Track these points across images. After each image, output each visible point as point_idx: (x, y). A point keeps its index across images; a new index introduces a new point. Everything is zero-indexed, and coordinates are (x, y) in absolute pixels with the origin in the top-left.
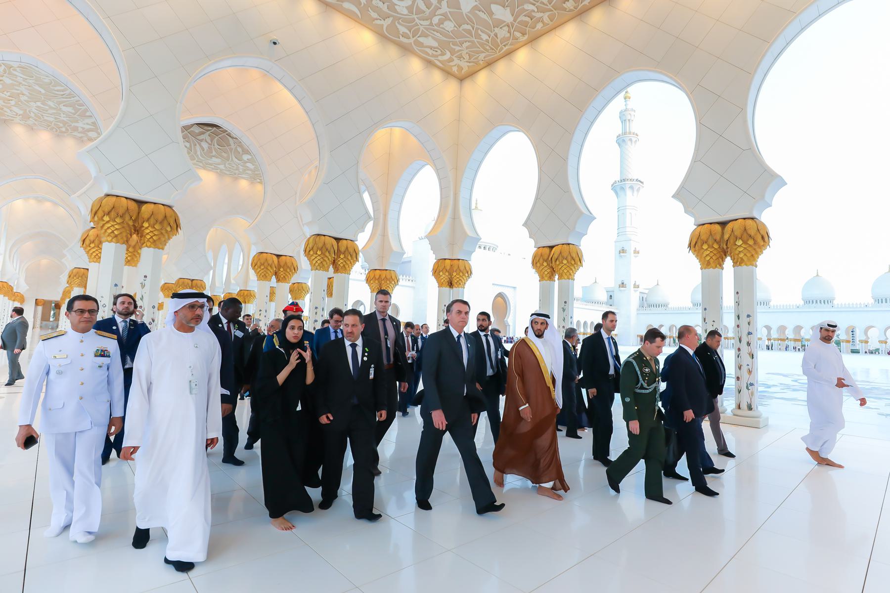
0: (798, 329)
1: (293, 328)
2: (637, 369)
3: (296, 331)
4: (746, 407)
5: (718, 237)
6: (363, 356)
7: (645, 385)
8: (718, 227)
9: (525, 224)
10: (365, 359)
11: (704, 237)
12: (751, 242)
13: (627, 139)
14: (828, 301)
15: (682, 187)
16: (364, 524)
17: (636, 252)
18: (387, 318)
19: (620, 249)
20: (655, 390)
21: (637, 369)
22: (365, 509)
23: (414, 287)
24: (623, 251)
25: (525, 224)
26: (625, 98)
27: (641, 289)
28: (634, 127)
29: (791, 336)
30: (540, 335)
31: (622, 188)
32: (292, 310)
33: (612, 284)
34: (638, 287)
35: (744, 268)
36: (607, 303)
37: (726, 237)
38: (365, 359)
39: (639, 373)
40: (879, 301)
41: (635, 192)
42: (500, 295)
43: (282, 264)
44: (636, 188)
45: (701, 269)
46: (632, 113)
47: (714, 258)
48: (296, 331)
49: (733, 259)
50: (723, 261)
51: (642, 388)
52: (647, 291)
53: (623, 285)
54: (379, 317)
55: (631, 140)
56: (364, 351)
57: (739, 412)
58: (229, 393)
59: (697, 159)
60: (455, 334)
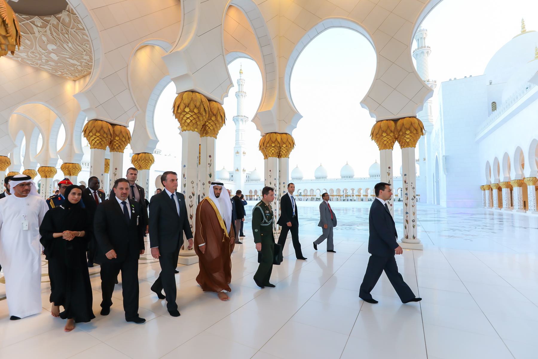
0: (359, 190)
1: (74, 194)
2: (262, 212)
3: (76, 196)
4: (412, 238)
5: (393, 129)
6: (132, 210)
7: (267, 221)
8: (392, 123)
10: (133, 212)
11: (384, 128)
12: (415, 132)
13: (240, 95)
14: (351, 177)
15: (368, 96)
16: (133, 326)
17: (244, 153)
18: (135, 185)
21: (262, 212)
22: (133, 315)
24: (238, 153)
27: (247, 172)
28: (245, 89)
29: (309, 194)
30: (217, 196)
31: (237, 120)
32: (65, 183)
33: (232, 169)
35: (410, 149)
37: (399, 128)
38: (133, 212)
39: (263, 214)
40: (317, 178)
41: (244, 123)
43: (117, 133)
45: (380, 150)
46: (243, 81)
47: (389, 142)
48: (76, 196)
49: (399, 142)
50: (394, 143)
51: (265, 223)
53: (237, 170)
56: (131, 207)
57: (406, 240)
59: (377, 79)
60: (170, 194)
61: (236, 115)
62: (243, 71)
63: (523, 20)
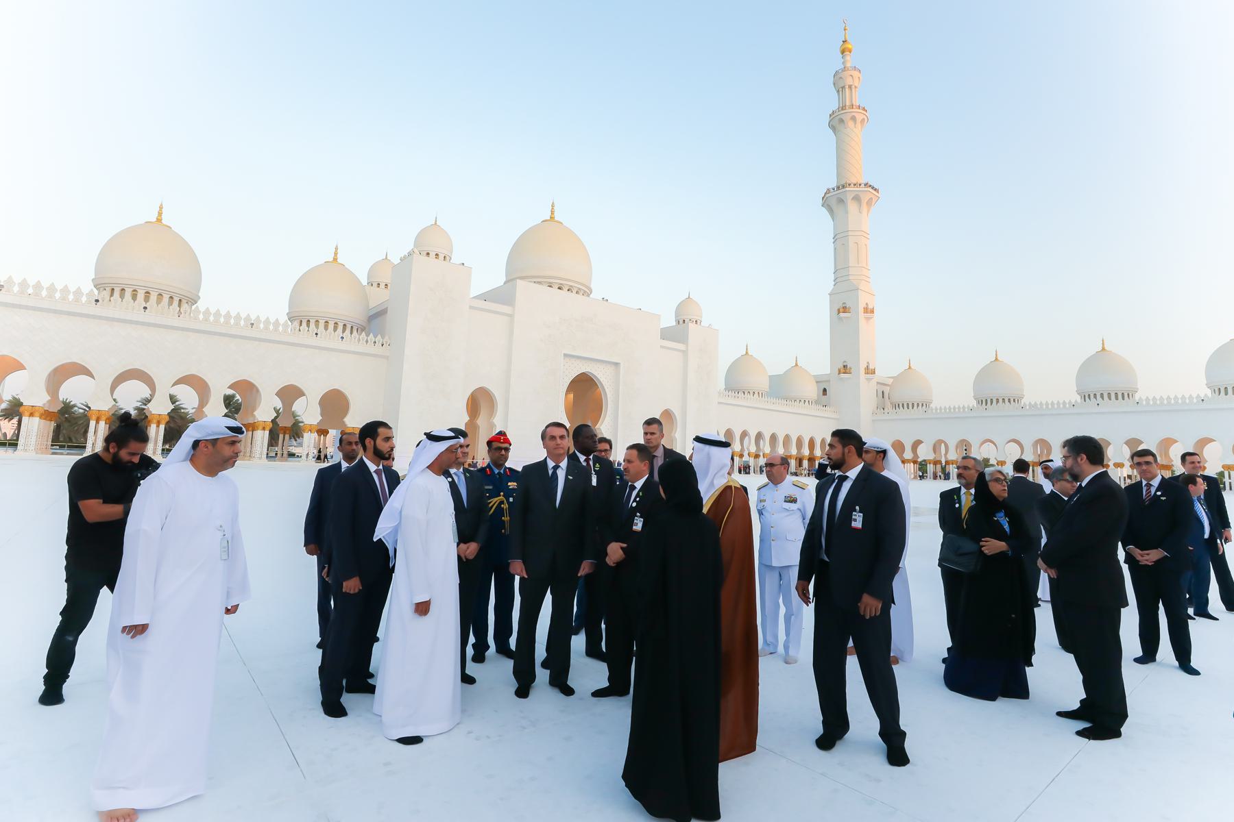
9: (1117, 734)
13: (847, 118)
17: (869, 311)
19: (841, 305)
23: (387, 358)
25: (1117, 734)
26: (843, 52)
36: (817, 402)
41: (859, 124)
46: (856, 74)
53: (845, 369)
55: (854, 118)
56: (638, 495)
58: (705, 510)
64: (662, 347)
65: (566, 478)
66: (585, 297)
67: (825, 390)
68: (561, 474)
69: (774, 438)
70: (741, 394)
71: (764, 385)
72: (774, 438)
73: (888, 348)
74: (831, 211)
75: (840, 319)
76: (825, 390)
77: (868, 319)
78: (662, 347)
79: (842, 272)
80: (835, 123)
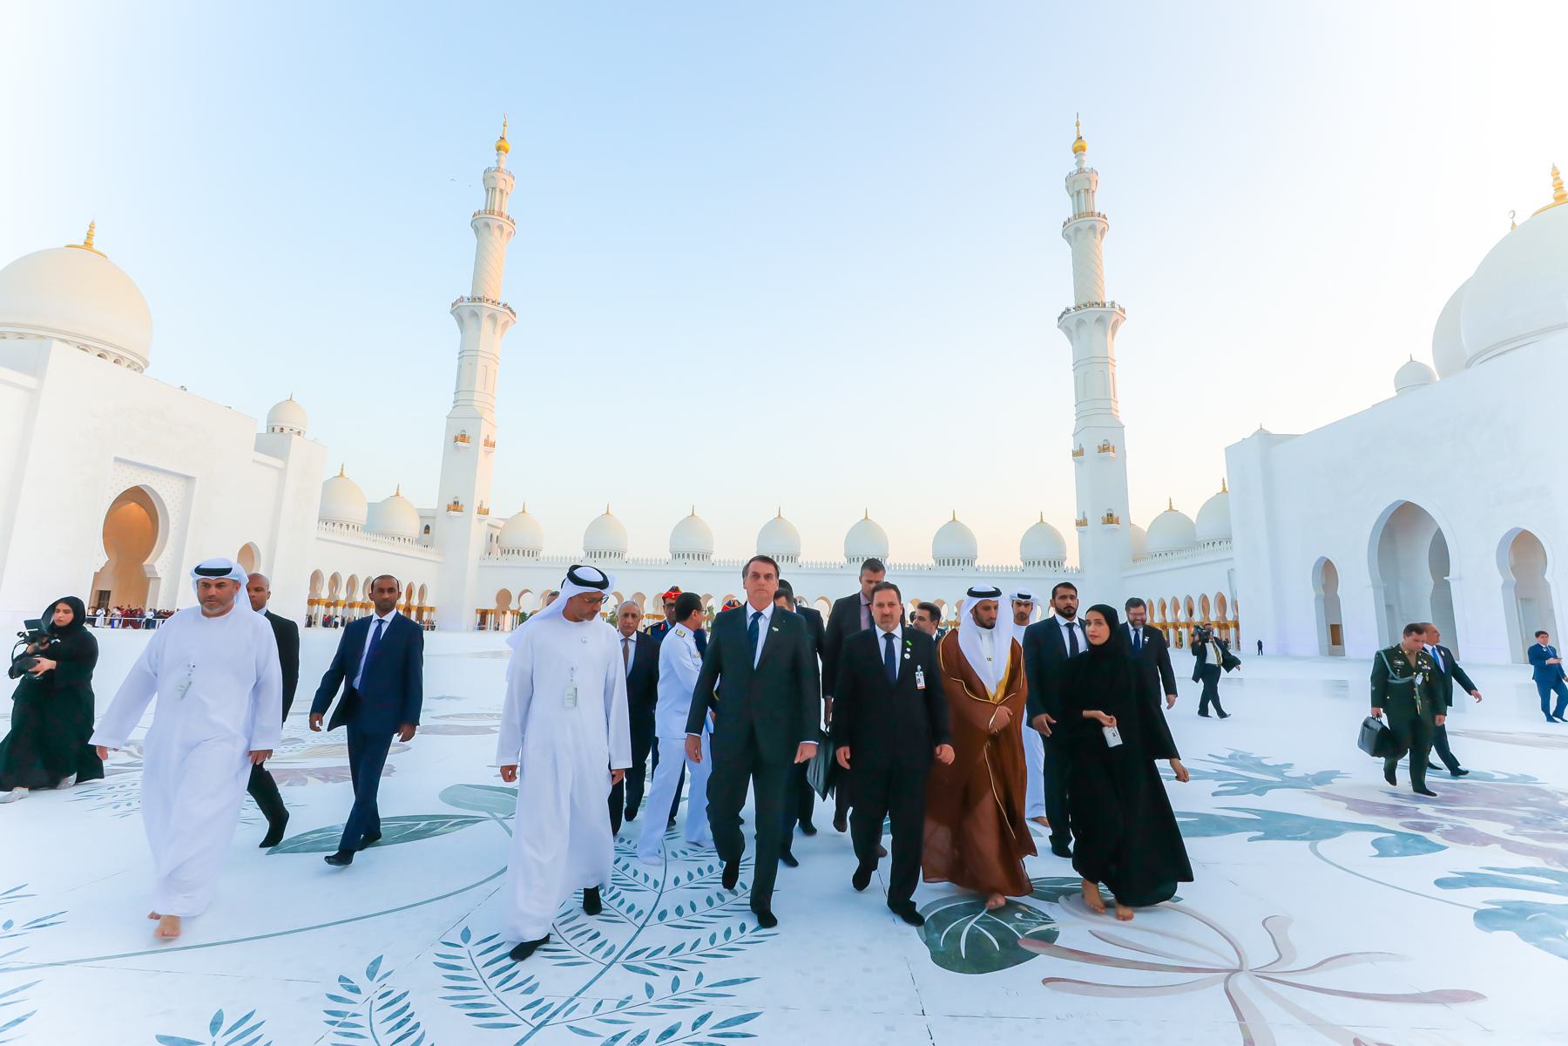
10: (907, 656)
14: (703, 556)
17: (489, 444)
19: (458, 433)
20: (1412, 683)
24: (463, 438)
26: (499, 149)
31: (475, 315)
34: (486, 512)
36: (418, 541)
38: (907, 656)
42: (138, 495)
44: (502, 319)
52: (501, 524)
53: (456, 506)
54: (863, 601)
55: (501, 228)
61: (468, 294)
62: (510, 143)
63: (1554, 168)
64: (1327, 572)
65: (770, 629)
66: (137, 374)
67: (427, 528)
68: (763, 626)
69: (335, 579)
70: (330, 525)
71: (360, 514)
72: (335, 579)
73: (502, 487)
74: (460, 321)
75: (457, 448)
76: (427, 528)
77: (488, 453)
78: (1327, 572)
79: (463, 394)
80: (480, 224)
